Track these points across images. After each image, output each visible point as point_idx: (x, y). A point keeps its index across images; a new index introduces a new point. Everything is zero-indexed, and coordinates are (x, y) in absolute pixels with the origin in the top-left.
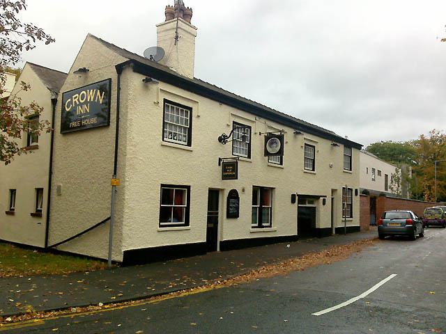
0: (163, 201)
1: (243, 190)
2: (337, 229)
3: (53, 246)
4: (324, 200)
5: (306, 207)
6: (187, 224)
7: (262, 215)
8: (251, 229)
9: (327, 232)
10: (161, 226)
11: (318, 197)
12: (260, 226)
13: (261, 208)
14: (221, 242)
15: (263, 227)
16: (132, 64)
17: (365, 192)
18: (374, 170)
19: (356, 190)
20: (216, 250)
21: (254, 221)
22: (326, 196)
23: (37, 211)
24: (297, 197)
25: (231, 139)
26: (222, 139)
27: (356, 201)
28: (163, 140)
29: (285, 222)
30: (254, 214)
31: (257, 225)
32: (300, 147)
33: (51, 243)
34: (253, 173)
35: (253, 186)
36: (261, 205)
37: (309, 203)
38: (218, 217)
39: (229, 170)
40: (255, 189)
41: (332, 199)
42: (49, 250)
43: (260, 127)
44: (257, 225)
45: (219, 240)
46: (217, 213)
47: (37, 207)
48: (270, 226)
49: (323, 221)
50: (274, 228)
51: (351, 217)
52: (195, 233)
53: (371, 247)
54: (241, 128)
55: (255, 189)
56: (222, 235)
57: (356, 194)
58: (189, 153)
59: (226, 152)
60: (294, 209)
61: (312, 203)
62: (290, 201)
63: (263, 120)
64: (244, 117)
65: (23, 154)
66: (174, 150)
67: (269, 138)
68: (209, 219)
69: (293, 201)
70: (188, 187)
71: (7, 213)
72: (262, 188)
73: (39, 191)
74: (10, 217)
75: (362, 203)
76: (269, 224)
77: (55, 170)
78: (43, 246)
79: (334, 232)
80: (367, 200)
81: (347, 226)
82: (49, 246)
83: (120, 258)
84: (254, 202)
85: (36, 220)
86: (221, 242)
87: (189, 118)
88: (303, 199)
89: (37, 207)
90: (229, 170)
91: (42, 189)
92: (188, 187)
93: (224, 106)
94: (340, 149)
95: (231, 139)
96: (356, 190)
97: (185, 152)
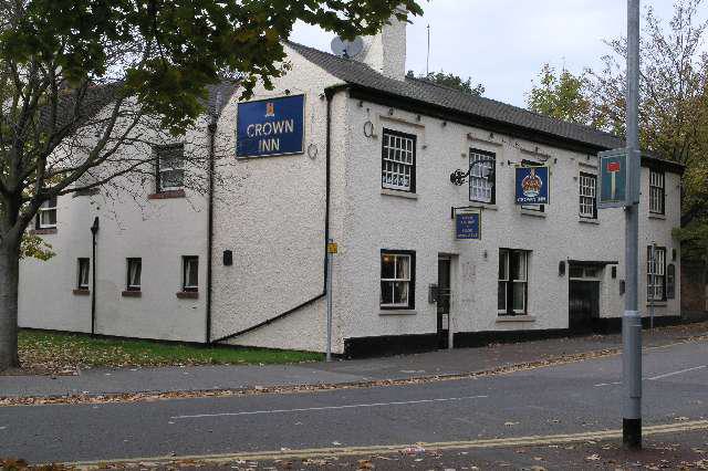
0: (500, 278)
1: (424, 147)
3: (221, 339)
4: (614, 270)
5: (583, 278)
7: (511, 295)
11: (601, 265)
12: (510, 313)
13: (511, 284)
15: (514, 314)
21: (501, 306)
22: (617, 263)
25: (467, 179)
26: (456, 178)
29: (548, 304)
30: (501, 296)
31: (505, 311)
32: (572, 179)
33: (217, 335)
34: (502, 228)
37: (587, 275)
39: (467, 225)
40: (504, 252)
43: (510, 153)
44: (505, 311)
52: (422, 321)
55: (504, 252)
58: (413, 202)
59: (460, 198)
60: (562, 286)
61: (593, 274)
62: (137, 299)
70: (413, 254)
71: (75, 292)
72: (512, 252)
74: (131, 301)
76: (522, 311)
77: (216, 229)
78: (202, 339)
82: (211, 341)
83: (341, 349)
84: (501, 275)
85: (188, 304)
88: (577, 267)
89: (129, 283)
90: (467, 225)
92: (413, 254)
95: (467, 179)
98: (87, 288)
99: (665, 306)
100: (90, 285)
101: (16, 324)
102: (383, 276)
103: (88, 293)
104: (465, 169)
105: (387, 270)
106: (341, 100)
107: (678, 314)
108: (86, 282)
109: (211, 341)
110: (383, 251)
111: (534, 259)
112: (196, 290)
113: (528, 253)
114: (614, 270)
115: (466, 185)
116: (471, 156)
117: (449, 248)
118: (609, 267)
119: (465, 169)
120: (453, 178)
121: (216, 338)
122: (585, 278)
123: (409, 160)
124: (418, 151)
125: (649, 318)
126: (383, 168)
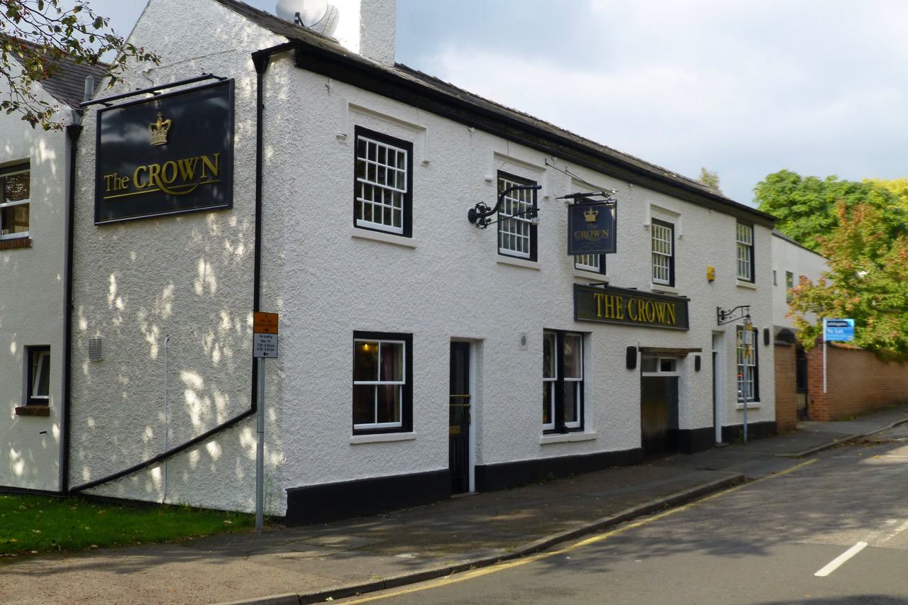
2: (726, 430)
4: (698, 360)
6: (408, 426)
8: (542, 437)
9: (706, 435)
10: (356, 432)
12: (560, 429)
13: (560, 384)
14: (477, 468)
16: (293, 51)
17: (785, 337)
18: (789, 275)
19: (766, 332)
20: (467, 489)
21: (548, 420)
22: (699, 350)
23: (30, 401)
24: (639, 354)
25: (494, 217)
27: (767, 356)
28: (356, 226)
35: (545, 330)
36: (561, 376)
38: (468, 408)
41: (714, 354)
42: (70, 495)
44: (551, 426)
45: (473, 462)
46: (467, 400)
47: (30, 392)
48: (581, 428)
49: (692, 416)
50: (589, 430)
51: (757, 399)
53: (828, 474)
54: (528, 189)
56: (479, 451)
57: (767, 342)
58: (406, 253)
60: (632, 382)
63: (561, 164)
64: (524, 161)
65: (893, 365)
66: (377, 248)
67: (579, 206)
68: (453, 411)
69: (631, 365)
70: (408, 338)
73: (36, 356)
75: (779, 364)
78: (55, 486)
79: (719, 439)
80: (790, 355)
81: (750, 422)
82: (71, 487)
83: (280, 507)
85: (35, 424)
86: (477, 468)
87: (405, 171)
89: (30, 392)
91: (47, 348)
92: (408, 338)
93: (335, 86)
94: (729, 225)
95: (494, 217)
96: (766, 332)
97: (398, 251)
98: (46, 401)
99: (757, 409)
100: (55, 400)
101: (283, 518)
102: (355, 379)
103: (45, 413)
104: (492, 203)
105: (363, 366)
106: (280, 71)
107: (772, 418)
108: (44, 389)
109: (71, 487)
110: (357, 334)
111: (487, 348)
112: (46, 401)
113: (479, 342)
114: (698, 360)
115: (493, 228)
116: (500, 183)
117: (567, 323)
118: (692, 356)
119: (492, 203)
120: (473, 217)
121: (76, 485)
122: (660, 373)
123: (400, 186)
124: (415, 168)
125: (741, 427)
126: (357, 193)
